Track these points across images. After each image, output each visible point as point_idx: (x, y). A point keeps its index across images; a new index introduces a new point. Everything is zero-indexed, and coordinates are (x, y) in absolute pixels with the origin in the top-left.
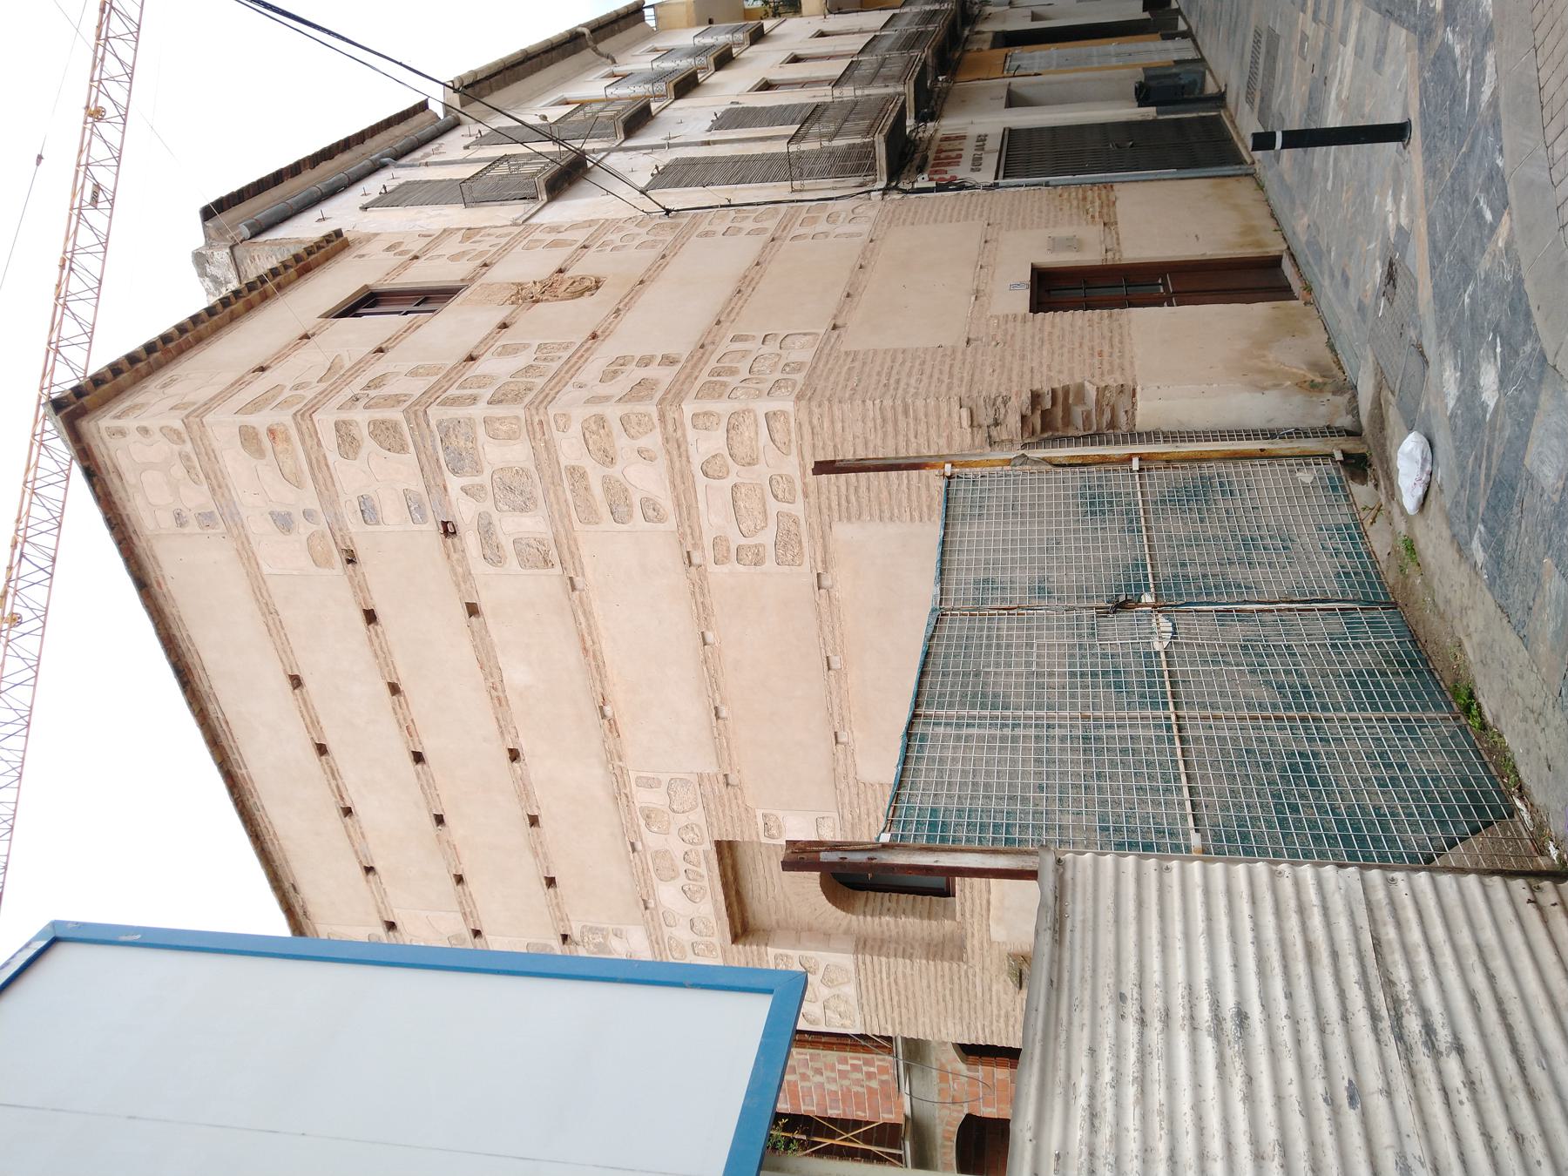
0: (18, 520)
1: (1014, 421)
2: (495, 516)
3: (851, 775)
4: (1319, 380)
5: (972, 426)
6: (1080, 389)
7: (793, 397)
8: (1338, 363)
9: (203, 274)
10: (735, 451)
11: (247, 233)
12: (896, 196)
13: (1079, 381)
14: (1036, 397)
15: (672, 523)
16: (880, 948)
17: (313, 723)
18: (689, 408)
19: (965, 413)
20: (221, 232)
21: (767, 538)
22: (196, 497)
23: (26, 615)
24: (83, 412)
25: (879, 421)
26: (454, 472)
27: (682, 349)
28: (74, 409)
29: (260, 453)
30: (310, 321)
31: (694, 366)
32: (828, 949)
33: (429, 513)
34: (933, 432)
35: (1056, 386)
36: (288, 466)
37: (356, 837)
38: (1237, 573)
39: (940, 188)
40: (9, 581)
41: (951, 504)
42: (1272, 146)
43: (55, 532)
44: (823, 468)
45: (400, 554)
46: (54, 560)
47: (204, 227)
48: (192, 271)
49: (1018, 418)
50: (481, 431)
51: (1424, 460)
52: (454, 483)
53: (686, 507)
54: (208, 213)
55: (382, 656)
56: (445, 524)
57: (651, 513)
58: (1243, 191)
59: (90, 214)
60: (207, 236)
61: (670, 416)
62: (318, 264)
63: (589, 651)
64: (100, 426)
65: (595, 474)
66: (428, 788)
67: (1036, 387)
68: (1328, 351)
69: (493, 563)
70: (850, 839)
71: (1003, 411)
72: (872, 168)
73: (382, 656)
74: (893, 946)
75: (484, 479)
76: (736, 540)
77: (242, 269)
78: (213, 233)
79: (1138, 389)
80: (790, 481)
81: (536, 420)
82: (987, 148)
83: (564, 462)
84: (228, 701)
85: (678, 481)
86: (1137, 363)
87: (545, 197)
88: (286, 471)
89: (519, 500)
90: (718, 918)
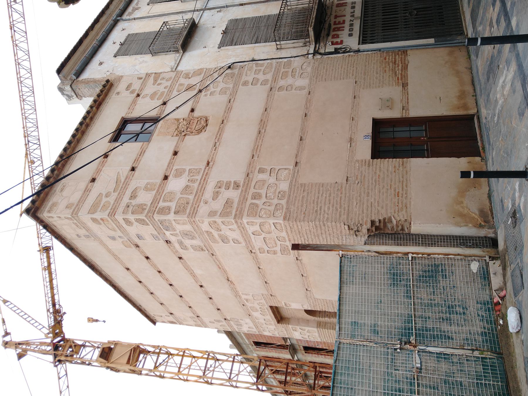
0: (24, 128)
1: (365, 231)
2: (183, 240)
3: (312, 297)
4: (483, 223)
5: (349, 229)
6: (390, 221)
7: (282, 218)
8: (491, 210)
9: (63, 94)
10: (263, 230)
11: (74, 77)
12: (319, 57)
13: (389, 215)
14: (373, 222)
15: (244, 244)
16: (325, 326)
17: (136, 277)
18: (245, 221)
19: (346, 227)
20: (65, 77)
21: (278, 249)
22: (82, 232)
23: (35, 160)
24: (37, 209)
25: (314, 227)
26: (167, 230)
27: (240, 178)
28: (35, 208)
29: (100, 224)
30: (104, 145)
31: (246, 191)
32: (308, 326)
33: (161, 239)
34: (335, 230)
35: (381, 218)
36: (110, 227)
37: (157, 299)
38: (445, 327)
39: (336, 51)
40: (27, 149)
41: (342, 272)
42: (470, 177)
43: (37, 130)
44: (295, 247)
45: (152, 245)
46: (39, 140)
47: (59, 76)
48: (59, 94)
49: (366, 230)
50: (173, 222)
51: (518, 326)
52: (168, 233)
53: (248, 241)
54: (59, 71)
55: (154, 266)
56: (167, 241)
57: (236, 241)
58: (460, 55)
59: (16, 6)
60: (61, 79)
61: (239, 221)
62: (103, 100)
63: (220, 267)
64: (44, 215)
65: (215, 234)
66: (176, 291)
67: (373, 218)
68: (488, 201)
69: (185, 250)
70: (313, 309)
71: (360, 228)
72: (308, 36)
73: (154, 266)
74: (329, 325)
75: (178, 232)
76: (266, 248)
77: (76, 92)
78: (63, 78)
79: (412, 223)
80: (283, 206)
81: (192, 220)
82: (355, 16)
83: (203, 230)
84: (107, 271)
85: (244, 235)
86: (412, 203)
87: (182, 51)
88: (110, 227)
89: (190, 237)
90: (273, 319)
